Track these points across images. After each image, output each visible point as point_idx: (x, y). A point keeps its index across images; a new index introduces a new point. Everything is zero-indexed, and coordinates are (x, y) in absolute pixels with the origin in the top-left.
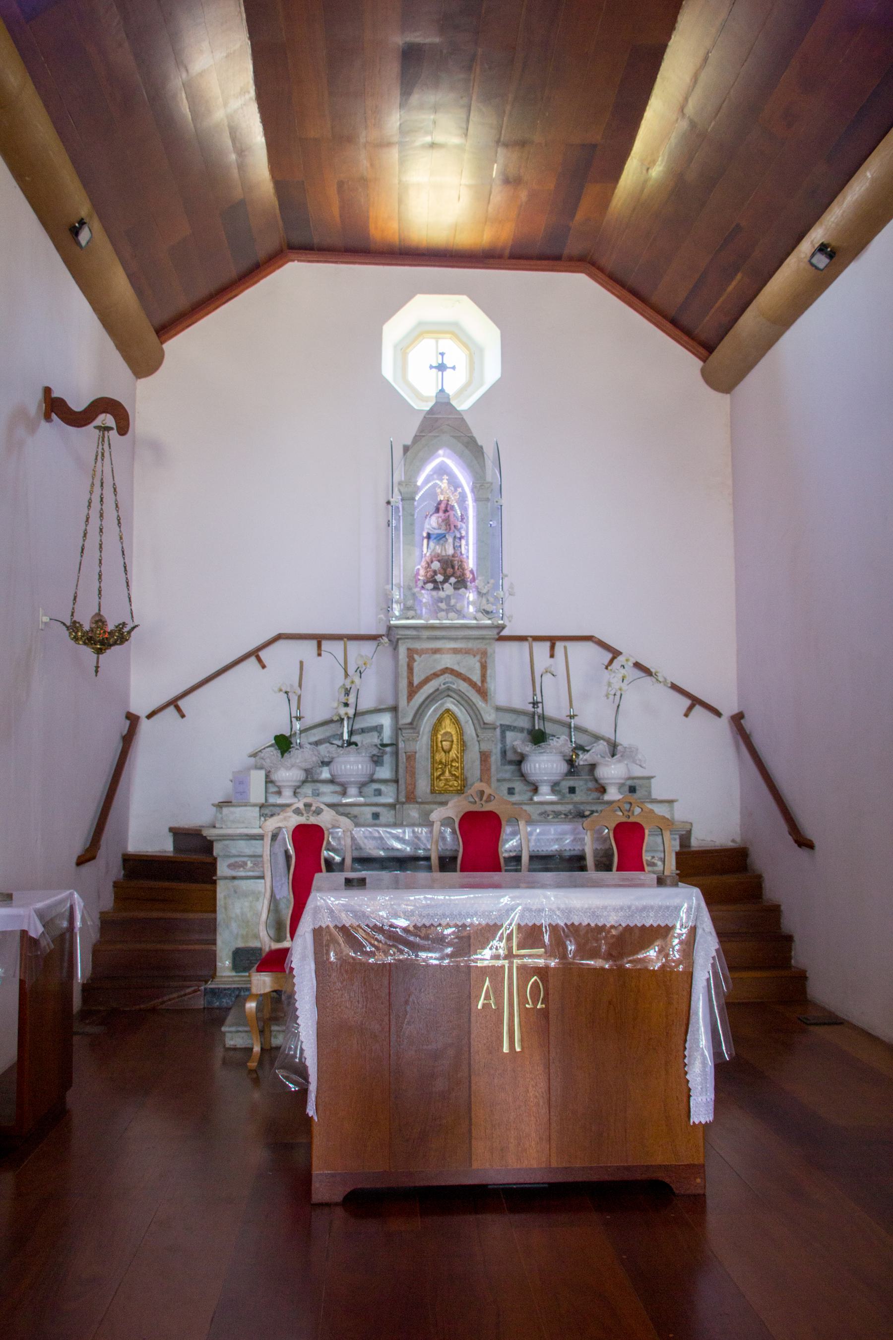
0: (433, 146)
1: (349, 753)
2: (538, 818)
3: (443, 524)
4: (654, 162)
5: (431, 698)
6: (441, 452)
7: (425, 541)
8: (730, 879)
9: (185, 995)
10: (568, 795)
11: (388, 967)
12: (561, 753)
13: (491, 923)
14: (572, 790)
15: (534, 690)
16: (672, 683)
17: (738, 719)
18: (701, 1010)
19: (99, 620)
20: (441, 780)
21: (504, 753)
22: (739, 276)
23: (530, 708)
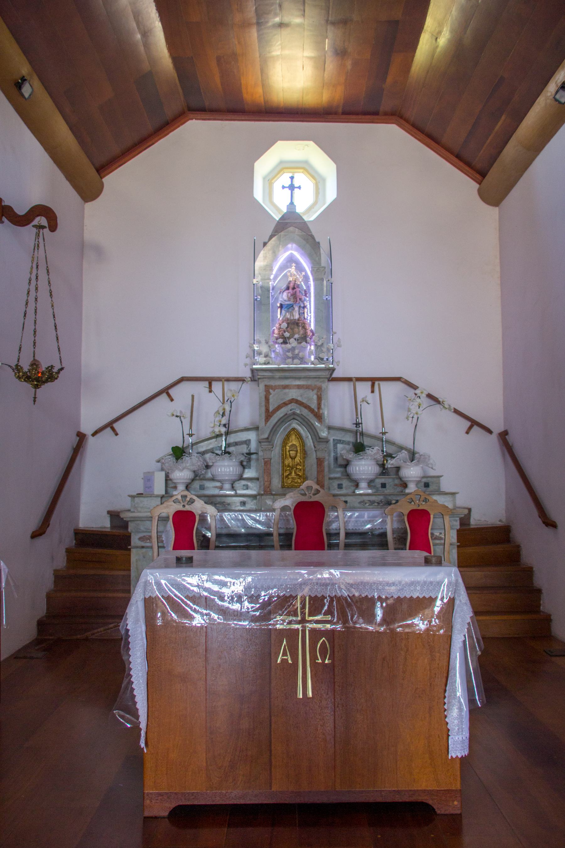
0: (281, 25)
1: (224, 459)
2: (358, 505)
3: (292, 297)
4: (440, 33)
5: (282, 421)
6: (290, 246)
7: (279, 310)
8: (499, 548)
9: (108, 629)
10: (380, 489)
11: (204, 629)
12: (375, 459)
13: (288, 595)
14: (384, 485)
15: (357, 415)
16: (455, 409)
17: (503, 436)
18: (458, 665)
19: (35, 364)
20: (289, 478)
21: (336, 459)
22: (503, 117)
23: (354, 428)
